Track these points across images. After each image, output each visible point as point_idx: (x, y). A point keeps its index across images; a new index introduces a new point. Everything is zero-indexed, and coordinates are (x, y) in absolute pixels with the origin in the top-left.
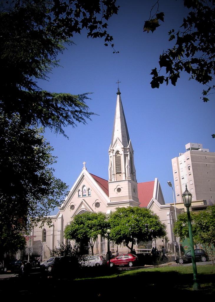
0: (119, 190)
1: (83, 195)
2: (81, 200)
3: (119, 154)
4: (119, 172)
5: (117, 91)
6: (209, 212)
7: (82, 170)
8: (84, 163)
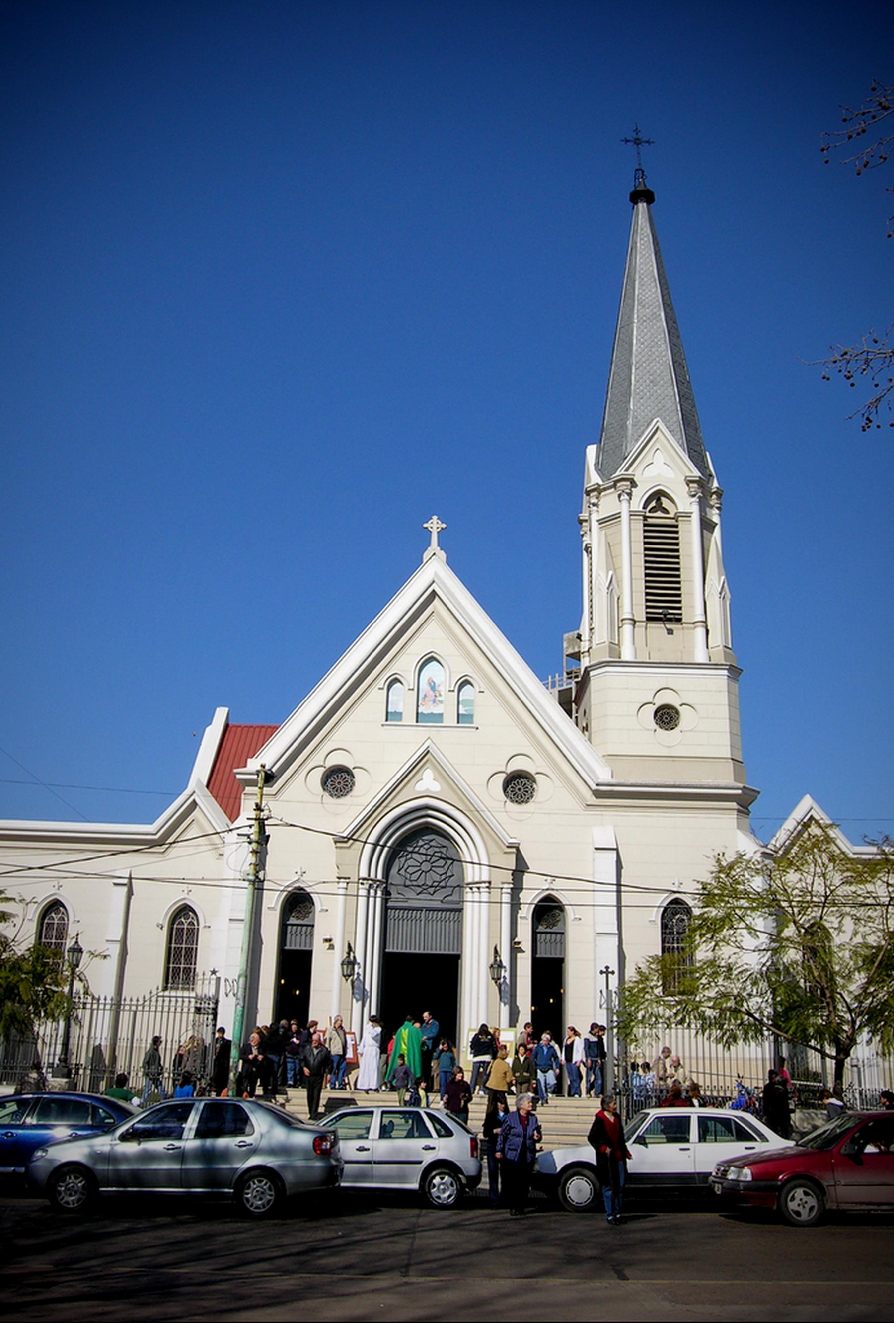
0: (666, 717)
2: (406, 743)
3: (665, 511)
7: (415, 563)
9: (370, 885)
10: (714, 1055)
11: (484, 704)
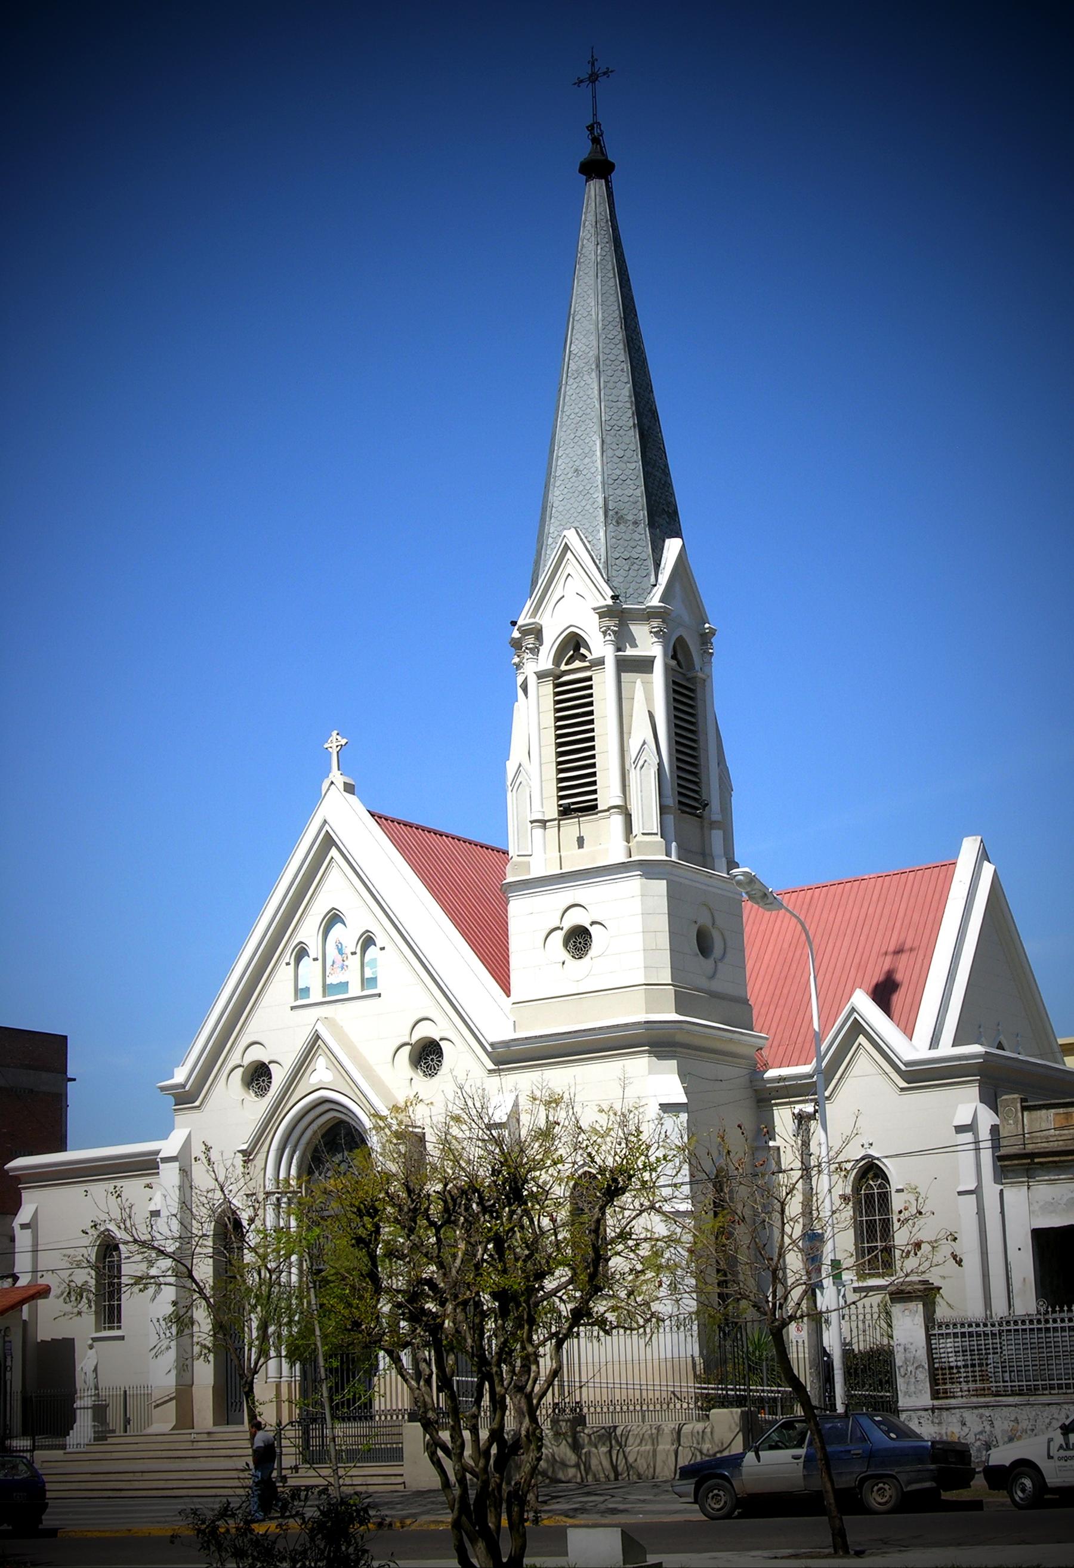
0: (578, 940)
1: (326, 988)
2: (304, 1023)
4: (577, 802)
5: (584, 150)
6: (802, 1460)
7: (315, 798)
8: (334, 742)
9: (278, 1199)
10: (642, 1357)
11: (388, 961)
